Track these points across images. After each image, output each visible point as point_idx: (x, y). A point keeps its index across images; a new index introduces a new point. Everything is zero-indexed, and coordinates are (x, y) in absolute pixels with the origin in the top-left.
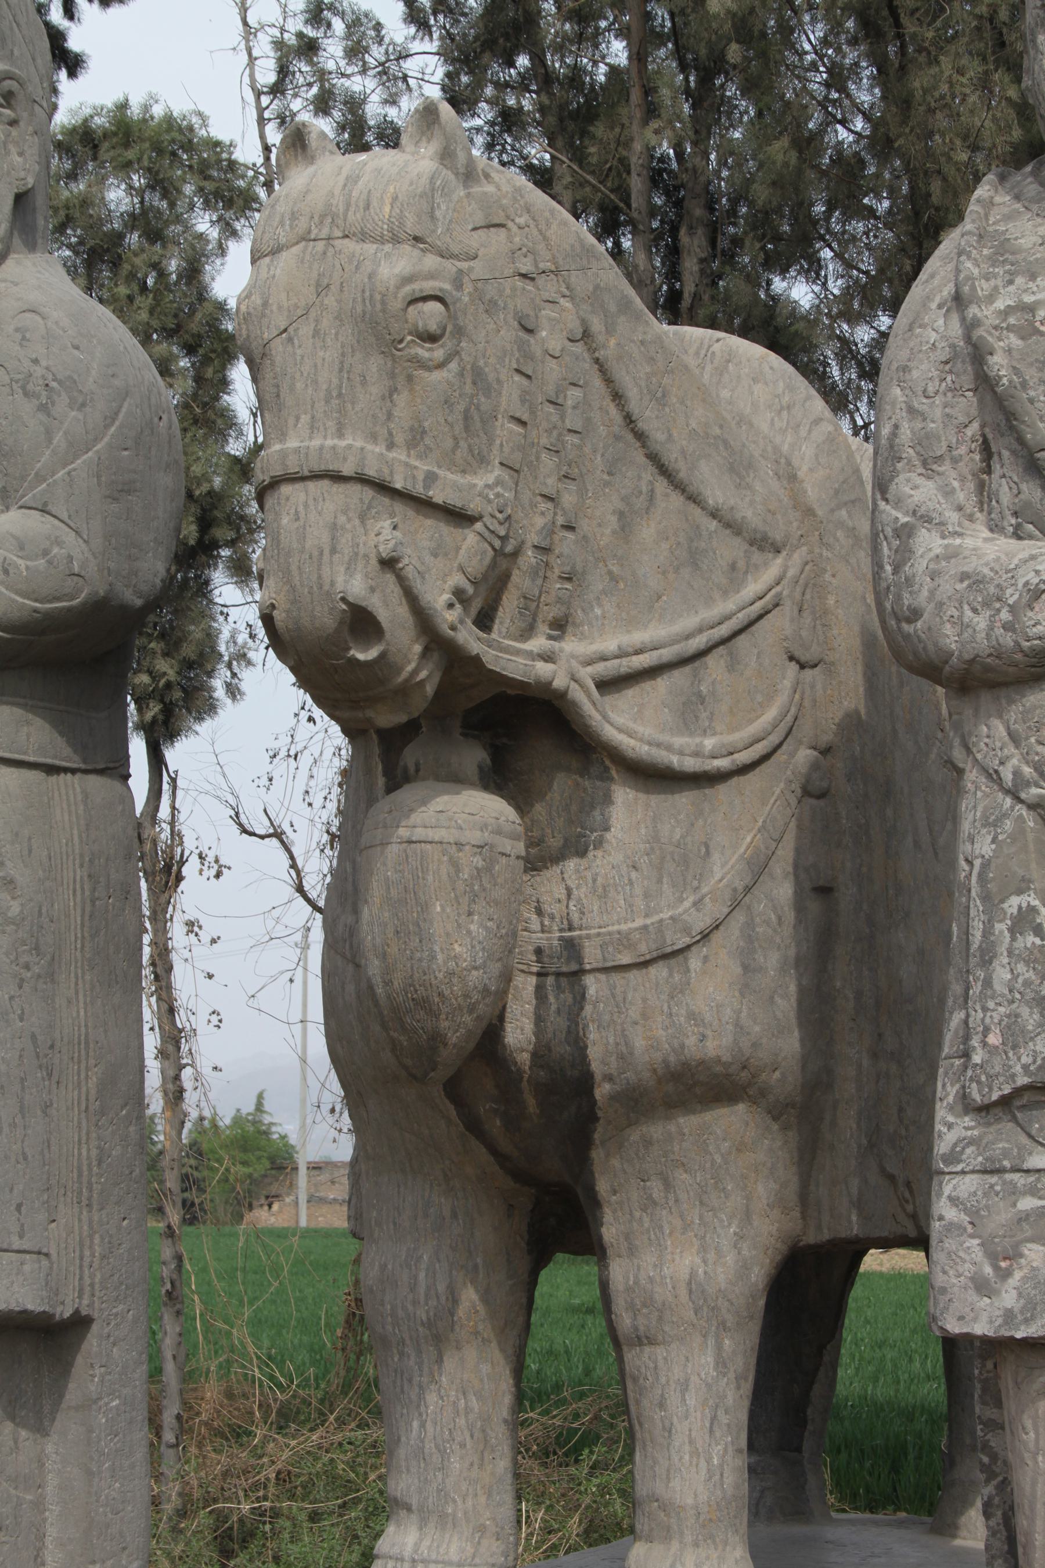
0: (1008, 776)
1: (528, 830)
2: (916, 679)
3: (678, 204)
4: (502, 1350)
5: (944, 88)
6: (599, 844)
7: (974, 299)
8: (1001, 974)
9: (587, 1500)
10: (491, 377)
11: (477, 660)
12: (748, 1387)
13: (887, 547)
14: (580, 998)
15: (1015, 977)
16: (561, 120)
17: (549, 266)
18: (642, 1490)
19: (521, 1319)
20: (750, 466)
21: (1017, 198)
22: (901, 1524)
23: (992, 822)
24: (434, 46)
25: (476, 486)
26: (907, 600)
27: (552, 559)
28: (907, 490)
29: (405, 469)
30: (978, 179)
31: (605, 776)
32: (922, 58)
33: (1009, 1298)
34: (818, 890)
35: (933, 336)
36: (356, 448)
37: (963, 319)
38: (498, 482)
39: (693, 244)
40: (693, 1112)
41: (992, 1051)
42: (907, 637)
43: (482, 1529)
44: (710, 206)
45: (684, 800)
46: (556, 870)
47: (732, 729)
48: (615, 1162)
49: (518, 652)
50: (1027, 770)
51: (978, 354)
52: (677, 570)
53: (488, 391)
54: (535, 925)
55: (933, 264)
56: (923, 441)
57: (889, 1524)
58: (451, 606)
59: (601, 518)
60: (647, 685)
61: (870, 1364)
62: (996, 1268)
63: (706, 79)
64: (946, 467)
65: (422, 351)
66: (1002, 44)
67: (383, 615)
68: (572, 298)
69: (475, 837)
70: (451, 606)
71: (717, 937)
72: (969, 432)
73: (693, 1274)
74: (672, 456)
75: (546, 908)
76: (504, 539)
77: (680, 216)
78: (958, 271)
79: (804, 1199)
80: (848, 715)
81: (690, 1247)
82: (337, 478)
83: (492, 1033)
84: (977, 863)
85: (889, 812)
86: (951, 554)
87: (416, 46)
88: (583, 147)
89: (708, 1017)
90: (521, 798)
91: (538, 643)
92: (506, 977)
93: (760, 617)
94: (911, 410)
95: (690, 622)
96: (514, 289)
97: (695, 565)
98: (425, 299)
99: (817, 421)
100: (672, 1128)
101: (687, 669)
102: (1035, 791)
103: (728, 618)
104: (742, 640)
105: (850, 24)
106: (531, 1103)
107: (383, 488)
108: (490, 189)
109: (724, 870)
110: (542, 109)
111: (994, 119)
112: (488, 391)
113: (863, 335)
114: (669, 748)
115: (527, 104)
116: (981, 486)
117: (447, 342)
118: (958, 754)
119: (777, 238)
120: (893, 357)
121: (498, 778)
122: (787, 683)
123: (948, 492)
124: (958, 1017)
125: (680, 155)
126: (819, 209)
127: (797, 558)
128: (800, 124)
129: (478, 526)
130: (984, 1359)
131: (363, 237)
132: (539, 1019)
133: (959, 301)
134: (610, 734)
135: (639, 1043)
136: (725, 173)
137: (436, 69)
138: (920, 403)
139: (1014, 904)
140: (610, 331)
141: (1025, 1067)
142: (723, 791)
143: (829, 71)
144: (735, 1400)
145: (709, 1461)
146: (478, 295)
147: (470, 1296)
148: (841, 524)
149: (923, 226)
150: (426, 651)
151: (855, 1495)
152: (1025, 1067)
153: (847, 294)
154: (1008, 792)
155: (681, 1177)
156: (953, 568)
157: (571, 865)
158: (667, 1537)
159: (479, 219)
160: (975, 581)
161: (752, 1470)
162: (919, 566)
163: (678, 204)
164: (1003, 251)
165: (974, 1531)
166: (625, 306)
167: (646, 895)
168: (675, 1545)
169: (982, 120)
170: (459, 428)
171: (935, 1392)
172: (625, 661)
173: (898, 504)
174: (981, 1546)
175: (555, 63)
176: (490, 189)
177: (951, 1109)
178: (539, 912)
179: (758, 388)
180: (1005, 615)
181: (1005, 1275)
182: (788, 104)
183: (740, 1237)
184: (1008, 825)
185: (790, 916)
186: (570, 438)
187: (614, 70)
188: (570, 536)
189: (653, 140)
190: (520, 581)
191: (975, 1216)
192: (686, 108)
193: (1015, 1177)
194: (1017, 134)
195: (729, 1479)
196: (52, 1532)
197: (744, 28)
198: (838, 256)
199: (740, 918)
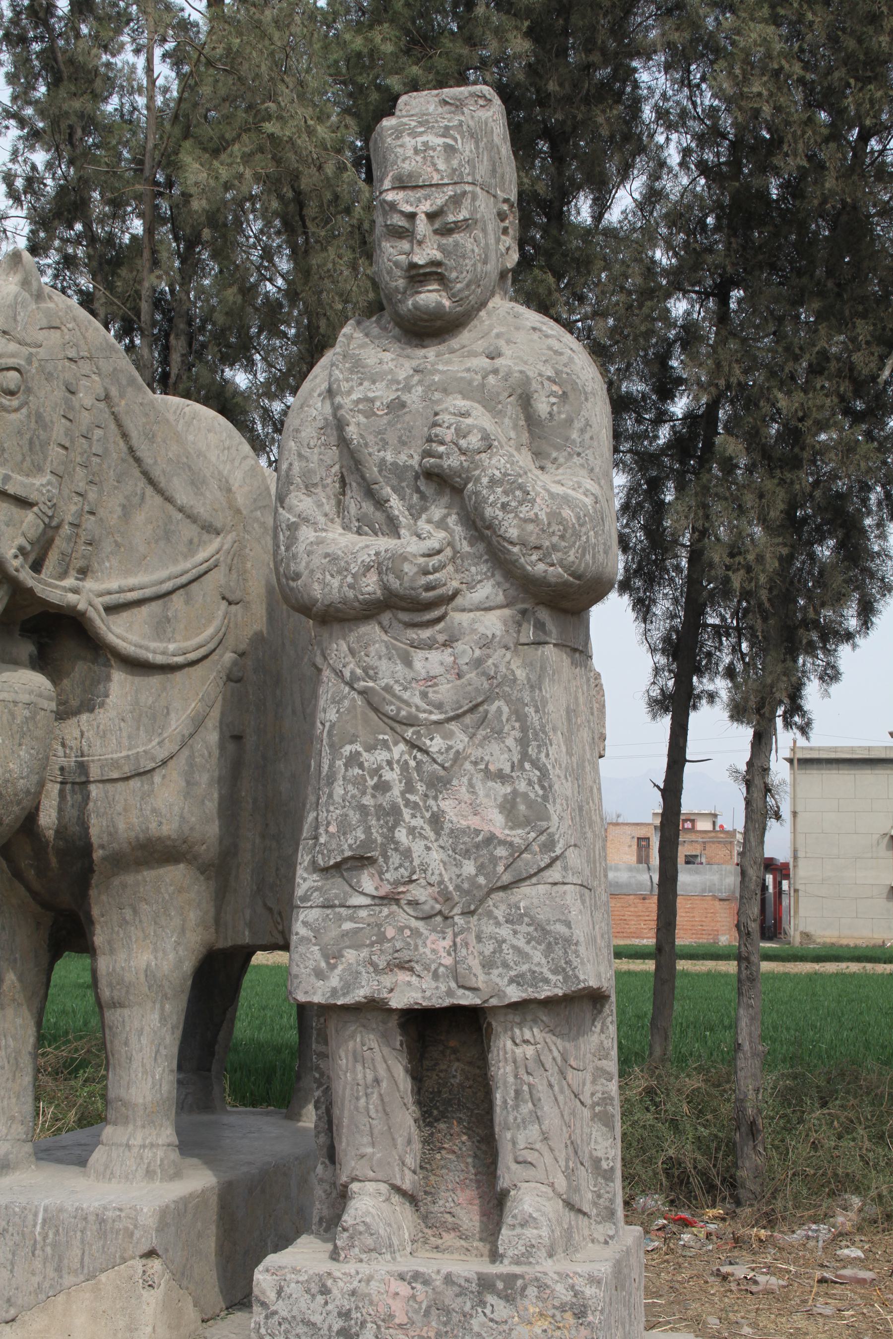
0: (347, 674)
1: (58, 695)
2: (297, 615)
3: (170, 320)
4: (30, 1010)
5: (330, 266)
6: (102, 705)
7: (339, 392)
8: (338, 791)
9: (81, 1101)
10: (47, 419)
11: (31, 591)
12: (179, 1033)
13: (283, 535)
14: (87, 798)
15: (346, 793)
16: (100, 264)
17: (86, 354)
18: (112, 1094)
19: (42, 992)
20: (204, 482)
21: (367, 335)
22: (268, 1114)
23: (337, 701)
24: (24, 213)
25: (35, 485)
26: (293, 567)
27: (80, 531)
28: (295, 502)
30: (347, 319)
31: (108, 665)
32: (318, 247)
33: (334, 981)
34: (233, 738)
35: (315, 413)
37: (332, 404)
38: (49, 483)
39: (178, 345)
40: (153, 868)
41: (332, 836)
42: (292, 589)
43: (12, 1118)
44: (190, 322)
45: (155, 681)
46: (74, 720)
47: (186, 639)
48: (104, 898)
49: (57, 587)
50: (359, 671)
51: (340, 425)
52: (157, 542)
53: (45, 427)
54: (61, 752)
55: (316, 369)
56: (306, 474)
57: (261, 1114)
58: (16, 557)
59: (111, 507)
60: (136, 611)
61: (254, 1020)
62: (328, 963)
63: (190, 246)
64: (319, 490)
66: (365, 243)
68: (99, 375)
69: (26, 698)
70: (16, 557)
71: (171, 763)
72: (333, 470)
73: (148, 965)
75: (68, 742)
76: (51, 518)
77: (171, 328)
78: (330, 375)
79: (217, 921)
80: (256, 634)
81: (147, 950)
83: (31, 817)
84: (327, 725)
85: (278, 692)
86: (320, 542)
87: (12, 212)
88: (113, 282)
89: (164, 811)
90: (55, 677)
91: (70, 582)
92: (41, 784)
93: (206, 573)
94: (300, 455)
95: (164, 574)
96: (64, 367)
97: (168, 540)
98: (8, 369)
99: (245, 458)
100: (140, 877)
101: (160, 602)
102: (362, 683)
103: (186, 572)
105: (277, 222)
106: (54, 861)
108: (51, 305)
109: (177, 723)
110: (89, 257)
111: (358, 286)
112: (45, 427)
113: (277, 407)
114: (147, 649)
115: (80, 254)
116: (339, 503)
118: (319, 660)
119: (229, 346)
120: (291, 422)
121: (41, 662)
122: (220, 613)
123: (320, 505)
124: (312, 816)
125: (172, 291)
126: (254, 330)
127: (230, 538)
128: (245, 279)
129: (35, 509)
130: (319, 1016)
132: (60, 810)
133: (330, 393)
135: (121, 826)
136: (199, 304)
137: (25, 228)
138: (306, 452)
139: (347, 749)
140: (122, 396)
141: (350, 846)
142: (179, 676)
143: (263, 249)
144: (171, 1041)
145: (153, 1077)
146: (41, 369)
147: (11, 977)
148: (256, 520)
149: (315, 345)
151: (243, 1097)
152: (350, 846)
153: (267, 384)
154: (347, 683)
156: (321, 550)
157: (84, 717)
158: (126, 1121)
159: (44, 323)
160: (333, 559)
161: (180, 1082)
162: (300, 548)
163: (170, 320)
164: (357, 365)
165: (309, 1118)
166: (132, 382)
167: (129, 737)
168: (131, 1127)
169: (351, 286)
170: (26, 448)
171: (292, 1036)
172: (122, 595)
173: (290, 510)
174: (312, 1125)
175: (99, 231)
176: (51, 305)
177: (306, 869)
178: (63, 745)
179: (211, 436)
180: (349, 579)
181: (333, 967)
182: (237, 266)
183: (178, 943)
184: (346, 703)
185: (216, 752)
186: (95, 460)
187: (134, 237)
188: (92, 518)
189: (155, 282)
190: (60, 544)
191: (317, 932)
192: (177, 264)
193: (342, 910)
194: (371, 295)
195: (165, 1088)
197: (213, 219)
198: (264, 359)
199: (186, 752)
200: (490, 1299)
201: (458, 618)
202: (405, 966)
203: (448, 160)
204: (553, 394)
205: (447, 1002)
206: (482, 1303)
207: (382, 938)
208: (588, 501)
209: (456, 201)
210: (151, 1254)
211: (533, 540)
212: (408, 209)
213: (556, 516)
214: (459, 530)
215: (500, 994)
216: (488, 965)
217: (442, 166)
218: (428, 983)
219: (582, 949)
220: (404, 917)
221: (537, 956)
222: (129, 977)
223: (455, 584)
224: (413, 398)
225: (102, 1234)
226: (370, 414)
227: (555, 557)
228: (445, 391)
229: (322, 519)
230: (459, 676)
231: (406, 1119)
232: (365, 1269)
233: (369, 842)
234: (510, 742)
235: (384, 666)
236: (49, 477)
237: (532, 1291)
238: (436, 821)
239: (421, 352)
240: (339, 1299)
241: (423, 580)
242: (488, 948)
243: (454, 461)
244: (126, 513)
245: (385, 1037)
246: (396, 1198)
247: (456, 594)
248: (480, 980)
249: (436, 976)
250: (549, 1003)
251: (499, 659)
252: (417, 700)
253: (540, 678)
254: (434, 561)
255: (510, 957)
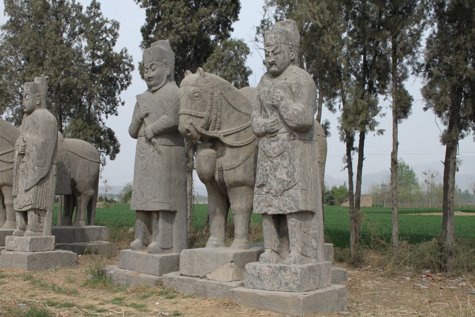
14: (223, 173)
29: (194, 112)
36: (188, 111)
45: (236, 149)
53: (206, 102)
59: (225, 115)
65: (196, 99)
67: (191, 130)
69: (207, 155)
71: (240, 166)
74: (236, 107)
82: (185, 114)
83: (213, 177)
91: (216, 131)
104: (247, 129)
107: (191, 115)
109: (242, 158)
112: (206, 102)
117: (199, 97)
131: (189, 85)
134: (225, 142)
135: (230, 179)
139: (261, 163)
142: (242, 148)
147: (218, 209)
150: (198, 134)
155: (238, 195)
156: (256, 122)
181: (259, 206)
196: (174, 236)
199: (244, 163)
200: (282, 271)
201: (279, 135)
202: (270, 206)
203: (275, 40)
204: (296, 87)
205: (277, 213)
206: (280, 272)
207: (267, 201)
208: (301, 109)
209: (276, 48)
210: (232, 262)
211: (289, 119)
212: (268, 51)
213: (293, 113)
214: (278, 117)
215: (286, 211)
216: (284, 206)
217: (274, 41)
218: (274, 209)
219: (301, 202)
220: (270, 196)
221: (292, 204)
222: (236, 209)
223: (278, 128)
224: (271, 90)
225: (224, 258)
226: (264, 94)
227: (293, 122)
228: (277, 88)
229: (257, 116)
230: (279, 147)
231: (275, 236)
232: (262, 265)
233: (264, 181)
234: (287, 160)
235: (266, 145)
236: (207, 112)
237: (288, 270)
238: (275, 177)
239: (274, 80)
240: (258, 270)
241: (271, 128)
242: (284, 202)
243: (276, 103)
244: (228, 116)
245: (269, 220)
246: (273, 252)
247: (278, 130)
248: (282, 209)
249: (275, 208)
250: (295, 213)
251: (286, 143)
252: (272, 152)
253: (294, 147)
254: (272, 124)
255: (288, 204)
